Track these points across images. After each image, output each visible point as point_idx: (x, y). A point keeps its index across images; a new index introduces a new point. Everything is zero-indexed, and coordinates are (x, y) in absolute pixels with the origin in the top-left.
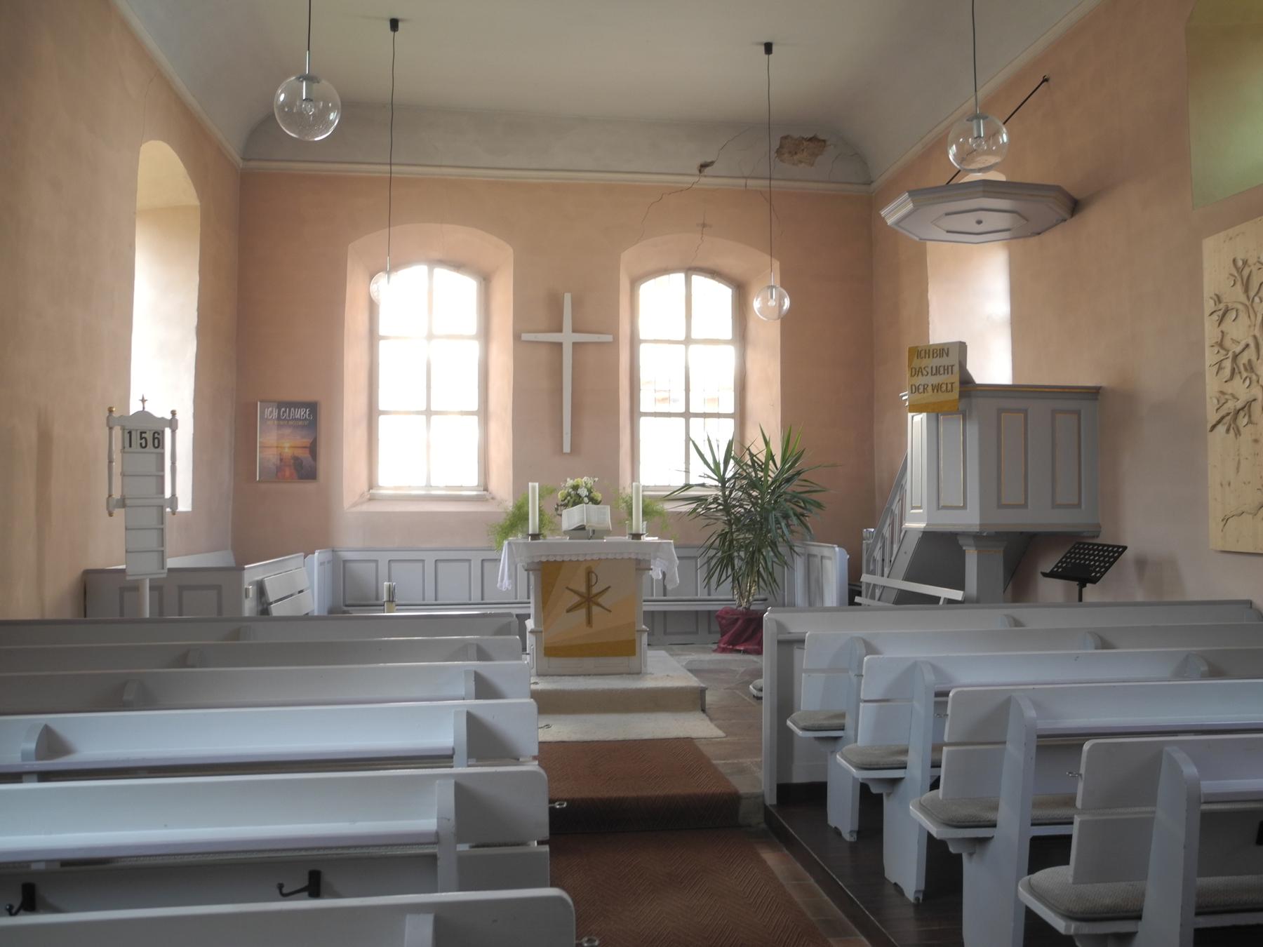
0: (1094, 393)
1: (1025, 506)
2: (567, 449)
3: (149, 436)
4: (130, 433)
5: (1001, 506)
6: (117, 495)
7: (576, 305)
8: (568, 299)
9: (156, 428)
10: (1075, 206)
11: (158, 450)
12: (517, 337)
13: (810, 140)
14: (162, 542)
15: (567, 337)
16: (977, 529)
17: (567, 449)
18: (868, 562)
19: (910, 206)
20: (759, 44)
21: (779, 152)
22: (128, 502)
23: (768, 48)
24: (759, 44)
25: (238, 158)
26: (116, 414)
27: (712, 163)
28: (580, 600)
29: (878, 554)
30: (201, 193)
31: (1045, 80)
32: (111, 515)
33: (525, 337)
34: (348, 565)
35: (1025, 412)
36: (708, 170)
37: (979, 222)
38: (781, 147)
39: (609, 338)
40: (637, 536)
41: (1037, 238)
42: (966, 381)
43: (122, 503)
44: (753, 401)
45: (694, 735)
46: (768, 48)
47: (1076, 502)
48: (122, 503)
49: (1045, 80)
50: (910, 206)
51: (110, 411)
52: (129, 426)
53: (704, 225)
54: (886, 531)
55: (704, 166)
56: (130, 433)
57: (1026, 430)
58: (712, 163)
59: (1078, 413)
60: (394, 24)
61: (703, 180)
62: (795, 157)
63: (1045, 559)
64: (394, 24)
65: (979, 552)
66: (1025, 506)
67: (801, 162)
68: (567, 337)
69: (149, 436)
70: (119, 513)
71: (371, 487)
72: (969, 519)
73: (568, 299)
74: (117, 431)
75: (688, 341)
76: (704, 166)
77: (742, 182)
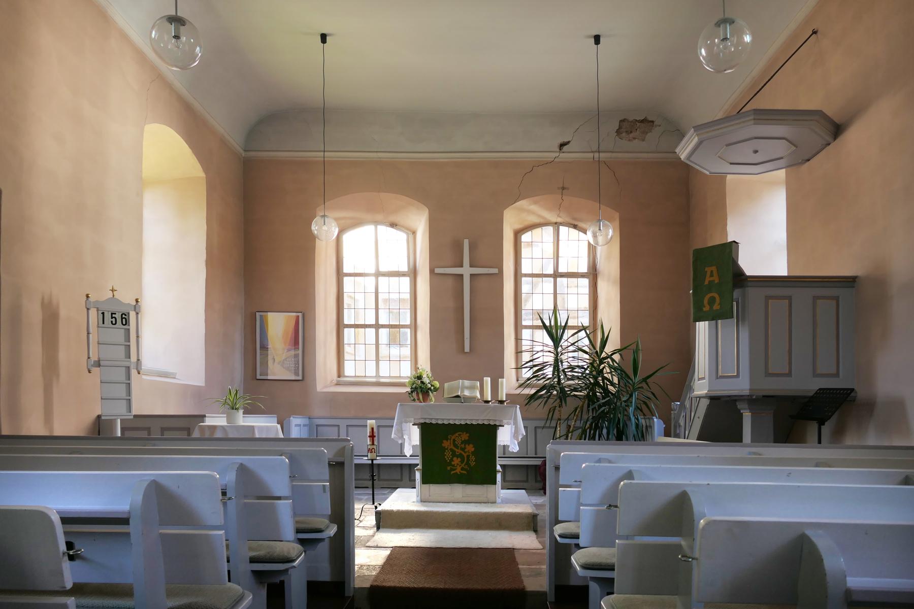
0: (850, 282)
1: (789, 374)
2: (467, 349)
3: (118, 316)
4: (103, 313)
5: (768, 374)
6: (94, 358)
7: (472, 248)
8: (466, 243)
9: (124, 310)
10: (837, 129)
11: (126, 327)
12: (432, 271)
13: (642, 121)
14: (129, 393)
15: (466, 271)
16: (747, 393)
17: (467, 349)
18: (675, 427)
19: (696, 140)
20: (589, 37)
21: (618, 132)
22: (102, 363)
23: (597, 39)
24: (589, 37)
25: (242, 151)
26: (92, 299)
27: (568, 143)
28: (458, 452)
29: (682, 422)
30: (206, 169)
31: (815, 32)
32: (89, 372)
33: (437, 271)
34: (525, 479)
35: (789, 298)
36: (565, 148)
37: (756, 152)
38: (620, 127)
39: (495, 271)
40: (487, 402)
41: (808, 163)
42: (739, 278)
43: (98, 364)
44: (602, 315)
45: (517, 546)
46: (597, 39)
47: (834, 372)
48: (98, 364)
49: (815, 32)
50: (729, 177)
51: (88, 296)
52: (103, 308)
53: (563, 188)
54: (687, 404)
55: (562, 145)
56: (103, 313)
57: (814, 337)
58: (568, 143)
59: (837, 299)
60: (324, 38)
61: (562, 155)
62: (631, 135)
63: (805, 415)
64: (324, 38)
65: (752, 414)
66: (789, 374)
67: (634, 138)
68: (466, 271)
69: (118, 316)
70: (95, 370)
71: (339, 376)
72: (741, 386)
73: (466, 243)
74: (93, 312)
75: (556, 275)
76: (562, 145)
77: (591, 155)
